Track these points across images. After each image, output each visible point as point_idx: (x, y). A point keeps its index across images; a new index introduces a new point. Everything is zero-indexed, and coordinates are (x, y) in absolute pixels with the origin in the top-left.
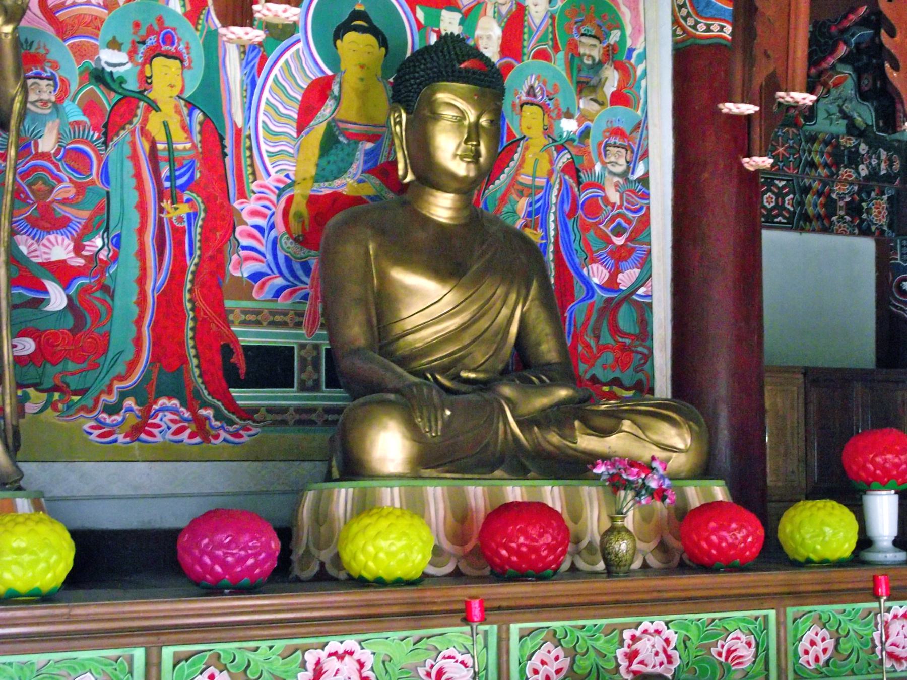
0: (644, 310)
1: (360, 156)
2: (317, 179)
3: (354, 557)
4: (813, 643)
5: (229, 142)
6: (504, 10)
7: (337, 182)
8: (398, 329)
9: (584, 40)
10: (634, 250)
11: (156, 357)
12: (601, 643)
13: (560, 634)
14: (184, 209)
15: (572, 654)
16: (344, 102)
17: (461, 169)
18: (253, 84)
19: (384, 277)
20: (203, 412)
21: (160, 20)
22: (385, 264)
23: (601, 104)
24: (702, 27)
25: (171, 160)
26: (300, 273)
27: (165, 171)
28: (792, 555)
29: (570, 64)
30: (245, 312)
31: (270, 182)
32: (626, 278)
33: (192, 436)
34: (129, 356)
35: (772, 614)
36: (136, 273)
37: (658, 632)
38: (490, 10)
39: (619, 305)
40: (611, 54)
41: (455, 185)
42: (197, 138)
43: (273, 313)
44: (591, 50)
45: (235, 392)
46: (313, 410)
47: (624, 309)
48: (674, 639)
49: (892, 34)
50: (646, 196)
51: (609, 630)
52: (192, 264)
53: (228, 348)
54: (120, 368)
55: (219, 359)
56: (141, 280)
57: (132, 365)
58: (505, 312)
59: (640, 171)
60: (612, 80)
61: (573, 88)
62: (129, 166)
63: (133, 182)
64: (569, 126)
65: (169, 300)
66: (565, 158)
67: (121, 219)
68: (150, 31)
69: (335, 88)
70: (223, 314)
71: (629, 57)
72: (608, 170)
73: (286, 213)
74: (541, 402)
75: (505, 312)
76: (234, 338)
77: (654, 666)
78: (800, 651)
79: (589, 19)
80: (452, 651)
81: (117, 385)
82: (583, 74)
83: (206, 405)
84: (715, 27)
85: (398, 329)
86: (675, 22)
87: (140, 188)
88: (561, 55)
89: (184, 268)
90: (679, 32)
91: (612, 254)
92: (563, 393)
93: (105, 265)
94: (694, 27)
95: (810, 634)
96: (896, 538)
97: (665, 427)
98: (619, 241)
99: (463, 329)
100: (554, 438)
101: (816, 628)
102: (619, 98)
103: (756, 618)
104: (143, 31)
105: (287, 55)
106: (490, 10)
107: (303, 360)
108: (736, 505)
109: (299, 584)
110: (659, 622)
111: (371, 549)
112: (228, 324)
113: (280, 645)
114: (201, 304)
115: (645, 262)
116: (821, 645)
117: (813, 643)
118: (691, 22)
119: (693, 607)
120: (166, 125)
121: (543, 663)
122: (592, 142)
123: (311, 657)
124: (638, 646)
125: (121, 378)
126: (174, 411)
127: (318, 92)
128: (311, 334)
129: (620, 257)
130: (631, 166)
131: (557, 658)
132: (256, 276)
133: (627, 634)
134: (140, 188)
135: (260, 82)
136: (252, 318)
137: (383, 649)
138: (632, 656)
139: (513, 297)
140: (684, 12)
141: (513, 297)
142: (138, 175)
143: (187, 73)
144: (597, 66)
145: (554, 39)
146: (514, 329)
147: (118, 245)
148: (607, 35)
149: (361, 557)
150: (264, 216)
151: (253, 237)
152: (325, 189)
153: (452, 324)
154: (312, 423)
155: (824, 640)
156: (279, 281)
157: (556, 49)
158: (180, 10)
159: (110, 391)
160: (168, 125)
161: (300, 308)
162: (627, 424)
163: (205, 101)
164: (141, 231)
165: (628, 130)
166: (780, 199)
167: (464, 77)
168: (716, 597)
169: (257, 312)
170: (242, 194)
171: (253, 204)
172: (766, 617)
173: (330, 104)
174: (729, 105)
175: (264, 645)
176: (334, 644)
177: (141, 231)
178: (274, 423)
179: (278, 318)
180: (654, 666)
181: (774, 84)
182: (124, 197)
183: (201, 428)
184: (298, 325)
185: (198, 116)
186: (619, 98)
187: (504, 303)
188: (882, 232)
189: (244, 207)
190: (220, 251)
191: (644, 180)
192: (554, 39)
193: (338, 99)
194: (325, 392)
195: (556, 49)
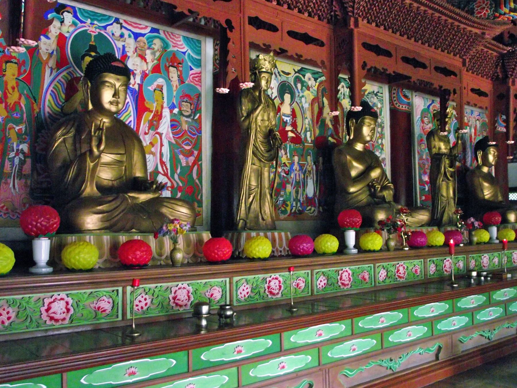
3: (251, 252)
4: (243, 290)
13: (147, 291)
28: (318, 253)
35: (372, 265)
37: (62, 299)
41: (510, 161)
48: (191, 290)
77: (61, 314)
78: (318, 284)
96: (48, 261)
103: (113, 291)
108: (215, 239)
109: (275, 258)
111: (257, 249)
119: (213, 277)
121: (140, 301)
131: (247, 289)
149: (254, 252)
155: (247, 289)
166: (12, 60)
167: (392, 100)
168: (239, 271)
180: (61, 314)
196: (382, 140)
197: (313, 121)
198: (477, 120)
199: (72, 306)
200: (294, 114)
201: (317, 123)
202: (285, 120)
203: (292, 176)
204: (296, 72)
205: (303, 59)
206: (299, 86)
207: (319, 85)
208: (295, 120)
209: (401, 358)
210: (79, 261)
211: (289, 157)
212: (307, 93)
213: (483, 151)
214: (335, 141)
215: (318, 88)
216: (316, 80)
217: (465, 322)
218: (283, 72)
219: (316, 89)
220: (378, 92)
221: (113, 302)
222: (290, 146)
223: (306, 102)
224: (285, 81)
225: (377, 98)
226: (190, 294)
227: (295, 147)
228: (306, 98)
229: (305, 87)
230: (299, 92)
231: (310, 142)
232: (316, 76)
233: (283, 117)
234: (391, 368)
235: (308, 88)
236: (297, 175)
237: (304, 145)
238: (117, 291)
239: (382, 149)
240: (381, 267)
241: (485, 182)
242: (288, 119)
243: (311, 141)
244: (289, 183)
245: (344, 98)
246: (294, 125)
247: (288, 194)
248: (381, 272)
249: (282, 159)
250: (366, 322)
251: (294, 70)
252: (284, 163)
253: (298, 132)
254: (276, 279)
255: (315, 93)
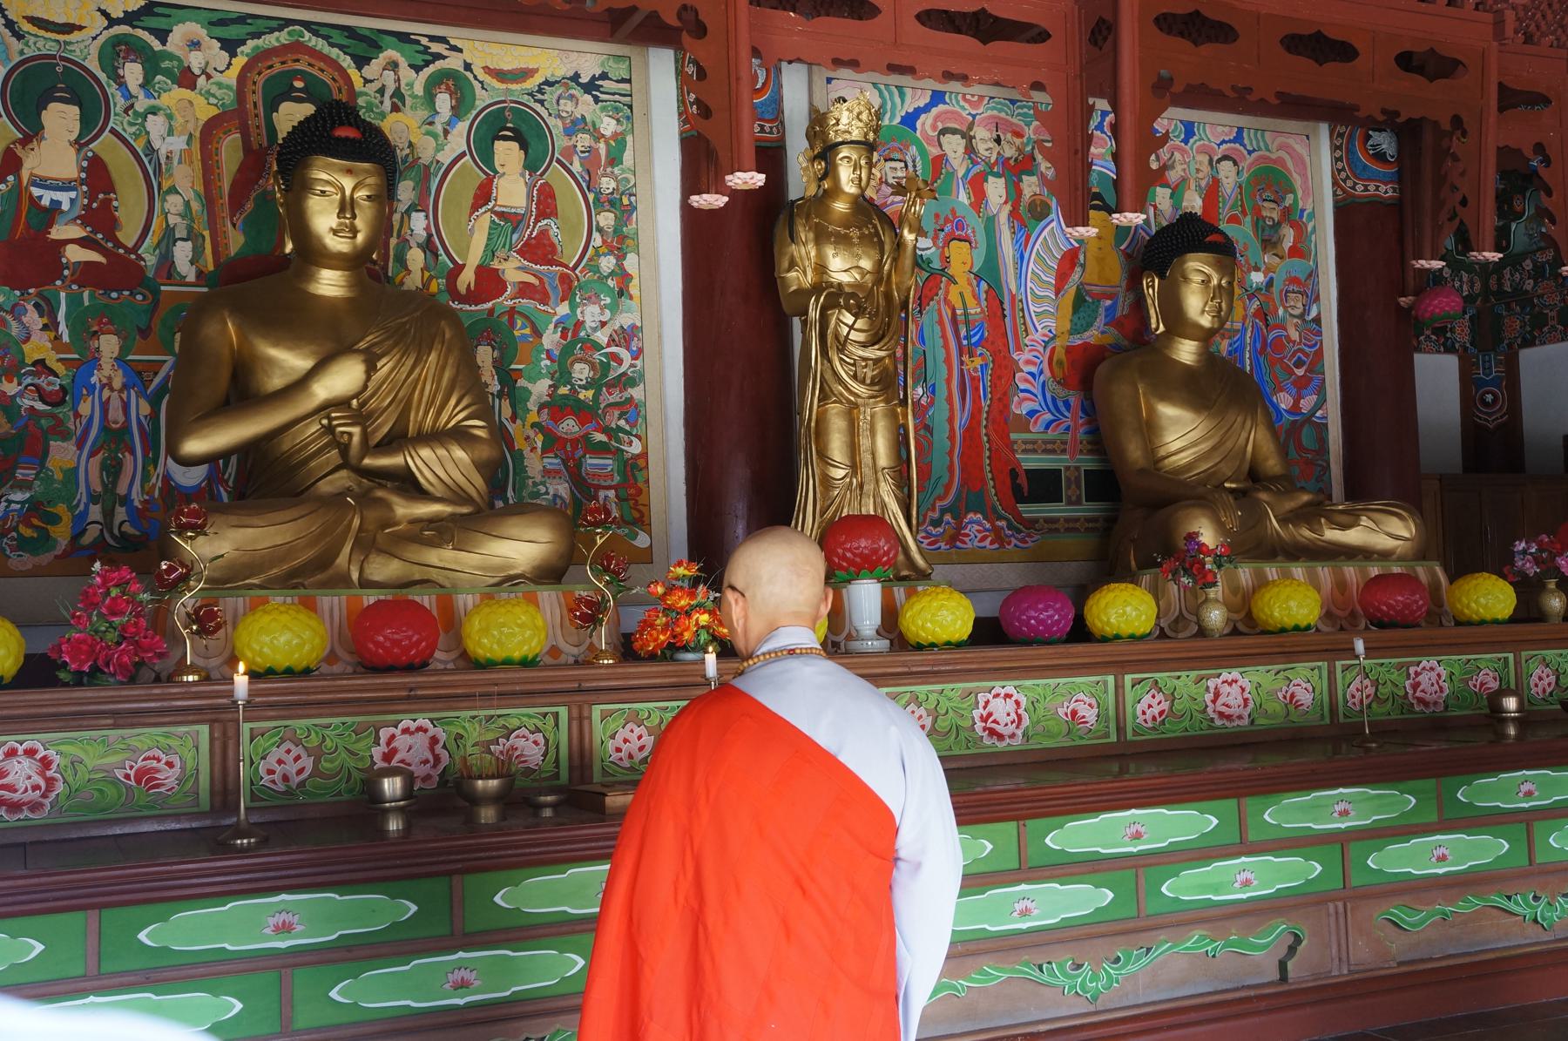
0: (1322, 428)
1: (1101, 311)
2: (1074, 331)
4: (1540, 679)
5: (1007, 306)
6: (1203, 183)
7: (1087, 334)
8: (1162, 452)
9: (1266, 204)
10: (1311, 381)
11: (964, 482)
12: (1394, 676)
14: (978, 362)
15: (1376, 683)
16: (1088, 269)
17: (1206, 321)
18: (1022, 257)
19: (1152, 411)
20: (999, 523)
21: (953, 211)
22: (1153, 401)
23: (1281, 258)
24: (1360, 188)
25: (967, 322)
26: (1063, 409)
27: (963, 332)
29: (1255, 225)
30: (1025, 442)
31: (1037, 337)
32: (1307, 403)
33: (992, 543)
34: (945, 480)
35: (1511, 656)
36: (946, 414)
37: (1432, 669)
38: (1193, 187)
39: (1302, 425)
40: (1287, 213)
42: (984, 304)
43: (1045, 442)
44: (1271, 212)
45: (1021, 507)
46: (1077, 520)
47: (1305, 430)
49: (1549, 193)
50: (1319, 333)
51: (1400, 667)
52: (985, 404)
53: (1014, 474)
54: (940, 491)
55: (1008, 481)
56: (951, 420)
57: (948, 487)
58: (1244, 435)
59: (1314, 313)
60: (1288, 237)
61: (1257, 245)
62: (937, 329)
63: (940, 342)
64: (1257, 278)
65: (971, 431)
66: (1256, 304)
67: (934, 373)
68: (947, 220)
69: (1081, 258)
70: (1010, 445)
71: (1301, 216)
72: (1287, 312)
73: (1051, 359)
74: (1289, 505)
75: (1244, 435)
76: (1018, 462)
77: (26, 790)
78: (1139, 712)
79: (1269, 186)
80: (1298, 681)
81: (938, 504)
82: (1267, 232)
83: (1001, 518)
84: (1372, 188)
85: (1162, 452)
86: (1335, 183)
87: (946, 346)
88: (1248, 219)
89: (980, 409)
90: (1339, 192)
91: (1294, 383)
92: (1306, 498)
93: (926, 408)
94: (1353, 188)
95: (1538, 671)
97: (1395, 520)
98: (1300, 372)
99: (1214, 448)
100: (1307, 533)
101: (1542, 667)
102: (1296, 252)
104: (941, 222)
105: (1045, 233)
106: (1193, 187)
107: (1068, 479)
110: (1433, 662)
112: (1013, 452)
113: (1194, 674)
114: (994, 437)
115: (1321, 390)
116: (1546, 681)
117: (1540, 679)
118: (1350, 183)
120: (961, 294)
122: (1275, 290)
123: (1211, 683)
124: (1420, 678)
125: (941, 498)
126: (979, 523)
127: (1070, 259)
128: (1072, 458)
129: (1301, 385)
130: (1306, 311)
132: (1032, 413)
133: (1412, 670)
134: (946, 346)
135: (1026, 256)
136: (1029, 447)
137: (1256, 679)
138: (1416, 686)
139: (1249, 423)
140: (1343, 175)
141: (1249, 423)
142: (944, 336)
143: (975, 252)
144: (1277, 226)
145: (1242, 206)
146: (1250, 448)
147: (933, 392)
148: (1284, 199)
150: (1034, 364)
151: (1027, 381)
152: (1077, 341)
153: (1205, 447)
154: (1057, 530)
156: (1049, 417)
157: (1244, 213)
158: (966, 202)
159: (933, 510)
160: (963, 295)
161: (1065, 437)
162: (1364, 521)
163: (989, 274)
164: (949, 381)
165: (1302, 277)
169: (1034, 442)
170: (1019, 348)
171: (1027, 355)
172: (1506, 659)
173: (1078, 269)
174: (1423, 262)
175: (1183, 674)
176: (1225, 675)
177: (949, 381)
178: (1050, 530)
179: (1049, 447)
181: (1465, 242)
182: (936, 353)
183: (999, 538)
184: (1064, 451)
185: (984, 286)
186: (1296, 252)
187: (1243, 427)
188: (1466, 349)
189: (1021, 358)
190: (1005, 394)
191: (1317, 320)
192: (1242, 206)
193: (1083, 266)
194: (1086, 505)
195: (1244, 213)
196: (621, 257)
197: (209, 199)
198: (1225, 158)
199: (444, 747)
200: (97, 176)
201: (236, 203)
202: (45, 202)
203: (85, 408)
204: (112, 22)
205: (1360, 114)
206: (133, 73)
207: (246, 69)
208: (107, 203)
209: (1118, 960)
210: (261, 653)
211: (66, 338)
212: (174, 96)
213: (1162, 277)
214: (103, 260)
215: (241, 78)
216: (230, 46)
217: (1440, 866)
218: (32, 20)
219: (234, 82)
220: (604, 76)
221: (547, 741)
222: (74, 301)
223: (170, 132)
224: (54, 57)
225: (597, 100)
226: (438, 748)
227: (104, 301)
228: (170, 117)
229: (167, 73)
230: (129, 96)
231: (191, 278)
232: (233, 32)
233: (36, 192)
234: (1535, 921)
235: (186, 79)
236: (115, 404)
237: (156, 292)
238: (556, 715)
239: (622, 292)
240: (1147, 685)
241: (1166, 398)
242: (64, 198)
243: (200, 274)
244: (65, 435)
245: (395, 108)
246: (100, 220)
247: (58, 476)
248: (1147, 699)
249: (26, 348)
250: (1284, 813)
251: (104, 13)
252: (40, 363)
253: (118, 244)
254: (30, 753)
255: (229, 98)
